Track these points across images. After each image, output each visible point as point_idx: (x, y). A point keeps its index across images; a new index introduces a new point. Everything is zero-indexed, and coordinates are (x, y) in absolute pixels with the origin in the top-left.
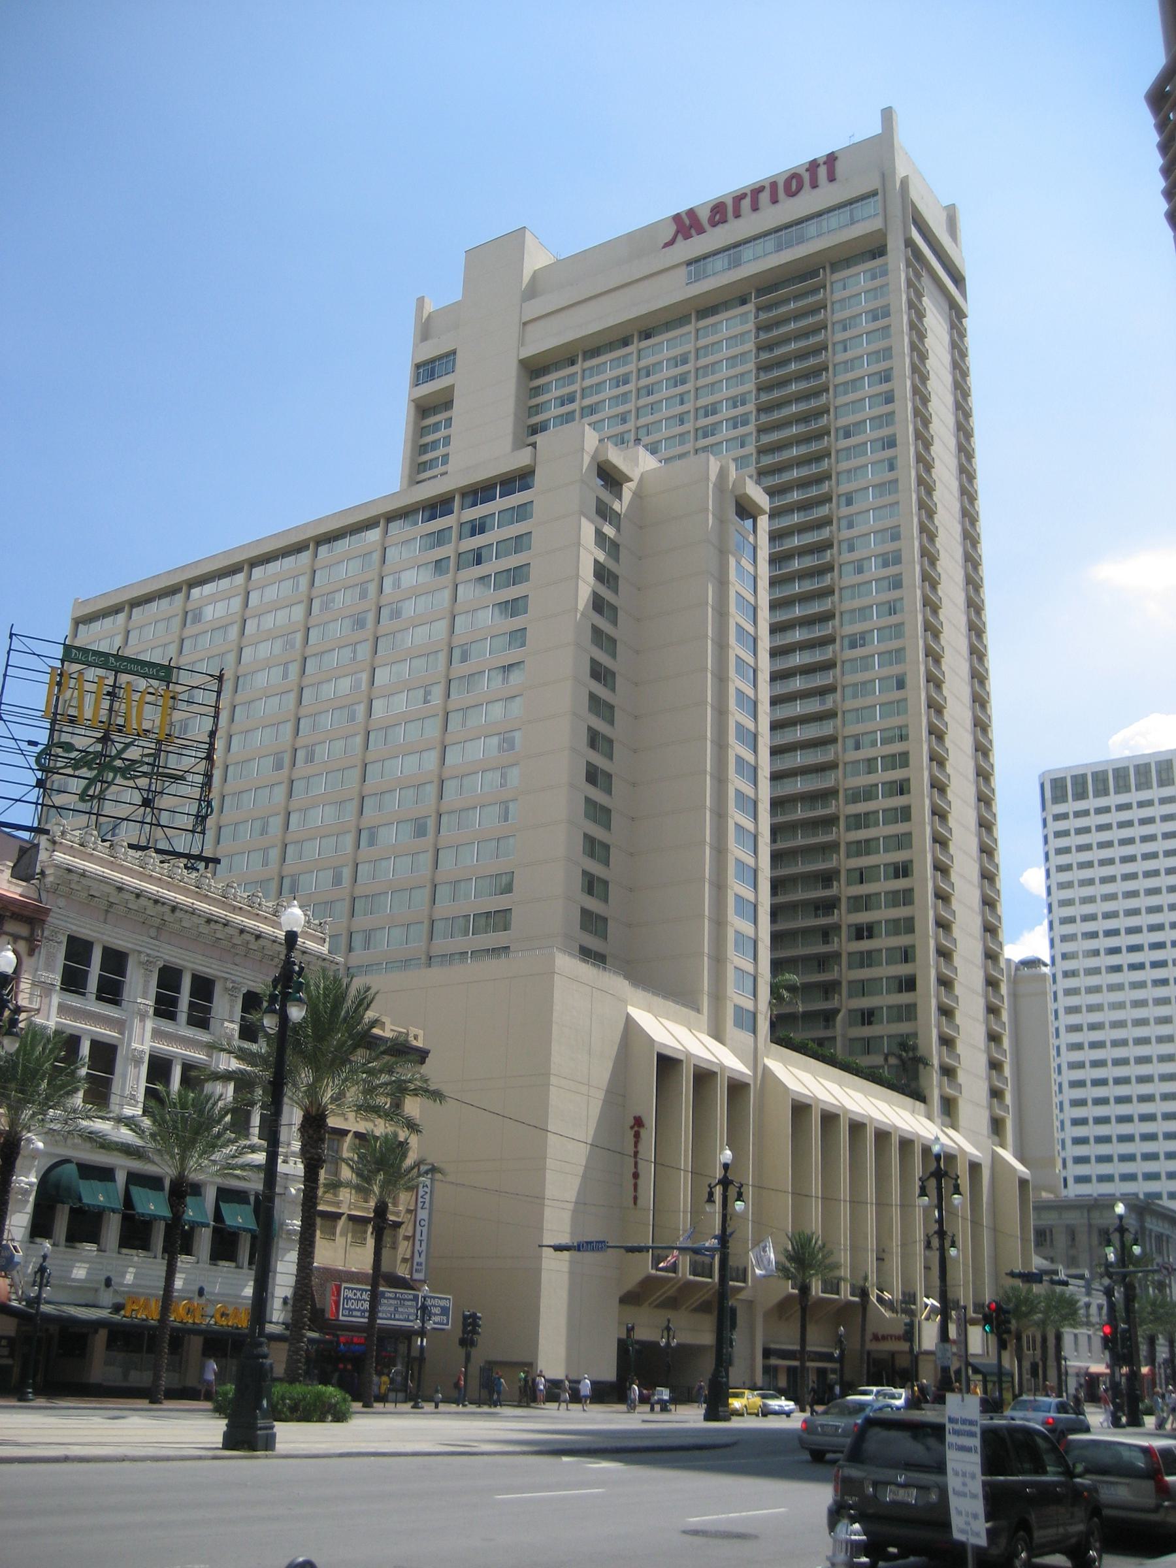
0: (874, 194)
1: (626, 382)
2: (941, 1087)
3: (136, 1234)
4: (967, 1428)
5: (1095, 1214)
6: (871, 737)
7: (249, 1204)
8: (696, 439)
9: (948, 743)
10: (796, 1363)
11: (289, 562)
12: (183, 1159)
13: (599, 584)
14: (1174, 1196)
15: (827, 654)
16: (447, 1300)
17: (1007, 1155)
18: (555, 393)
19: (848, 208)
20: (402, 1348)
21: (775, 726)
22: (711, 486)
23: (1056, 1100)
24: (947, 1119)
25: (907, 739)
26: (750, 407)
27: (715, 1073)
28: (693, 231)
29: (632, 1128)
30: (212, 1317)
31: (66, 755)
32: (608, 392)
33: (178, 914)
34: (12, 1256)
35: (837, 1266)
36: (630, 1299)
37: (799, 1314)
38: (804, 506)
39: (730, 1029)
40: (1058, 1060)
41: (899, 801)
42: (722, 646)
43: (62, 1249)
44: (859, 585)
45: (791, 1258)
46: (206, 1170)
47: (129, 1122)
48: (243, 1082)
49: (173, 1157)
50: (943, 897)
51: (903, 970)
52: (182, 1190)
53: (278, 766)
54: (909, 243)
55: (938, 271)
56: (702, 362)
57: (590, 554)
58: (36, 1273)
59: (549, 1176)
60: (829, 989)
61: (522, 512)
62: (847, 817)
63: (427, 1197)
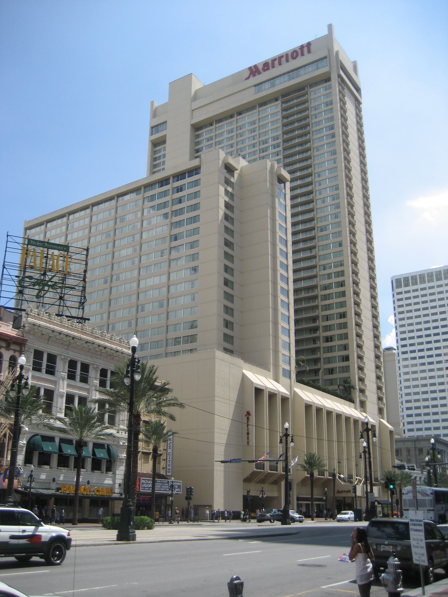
0: (326, 57)
1: (232, 132)
2: (359, 397)
3: (63, 461)
4: (418, 523)
5: (417, 443)
6: (330, 265)
7: (105, 449)
8: (260, 153)
9: (359, 267)
10: (310, 502)
11: (107, 204)
12: (81, 433)
13: (226, 210)
14: (445, 435)
15: (312, 234)
16: (179, 483)
17: (384, 422)
18: (205, 136)
19: (316, 63)
20: (163, 501)
21: (295, 262)
22: (268, 171)
23: (400, 401)
24: (362, 409)
25: (343, 266)
26: (280, 140)
27: (277, 394)
28: (256, 73)
29: (246, 416)
30: (93, 492)
31: (30, 281)
32: (226, 136)
33: (75, 340)
34: (20, 471)
35: (323, 466)
36: (247, 480)
37: (310, 483)
38: (302, 178)
39: (281, 377)
40: (400, 386)
41: (341, 289)
42: (274, 232)
43: (37, 468)
44: (323, 207)
45: (306, 463)
46: (90, 437)
47: (60, 420)
48: (101, 403)
49: (77, 431)
50: (358, 325)
51: (344, 353)
52: (80, 445)
53: (106, 282)
54: (340, 76)
55: (350, 87)
56: (261, 123)
57: (223, 198)
58: (29, 477)
59: (216, 435)
60: (316, 361)
61: (196, 183)
62: (321, 296)
63: (171, 444)
